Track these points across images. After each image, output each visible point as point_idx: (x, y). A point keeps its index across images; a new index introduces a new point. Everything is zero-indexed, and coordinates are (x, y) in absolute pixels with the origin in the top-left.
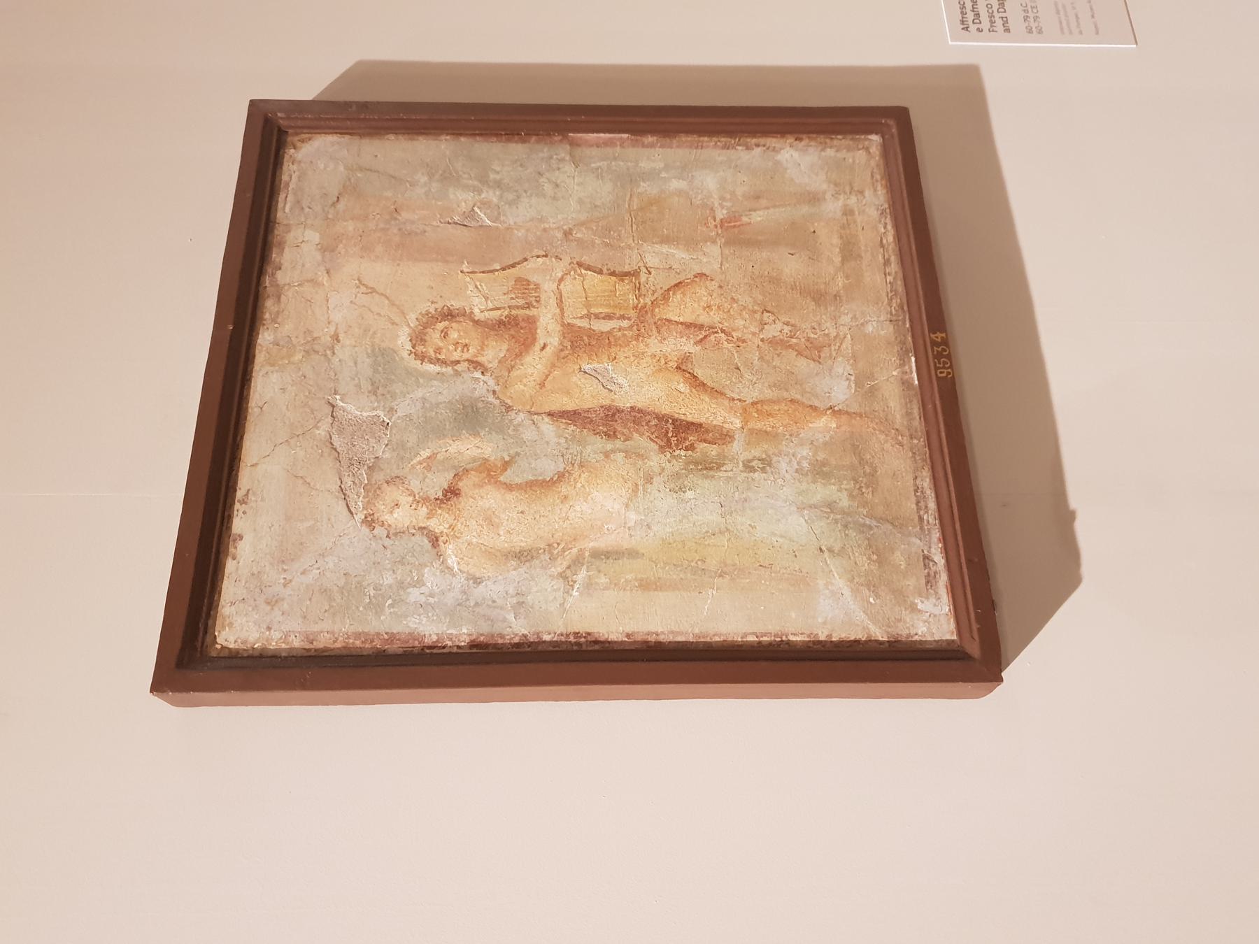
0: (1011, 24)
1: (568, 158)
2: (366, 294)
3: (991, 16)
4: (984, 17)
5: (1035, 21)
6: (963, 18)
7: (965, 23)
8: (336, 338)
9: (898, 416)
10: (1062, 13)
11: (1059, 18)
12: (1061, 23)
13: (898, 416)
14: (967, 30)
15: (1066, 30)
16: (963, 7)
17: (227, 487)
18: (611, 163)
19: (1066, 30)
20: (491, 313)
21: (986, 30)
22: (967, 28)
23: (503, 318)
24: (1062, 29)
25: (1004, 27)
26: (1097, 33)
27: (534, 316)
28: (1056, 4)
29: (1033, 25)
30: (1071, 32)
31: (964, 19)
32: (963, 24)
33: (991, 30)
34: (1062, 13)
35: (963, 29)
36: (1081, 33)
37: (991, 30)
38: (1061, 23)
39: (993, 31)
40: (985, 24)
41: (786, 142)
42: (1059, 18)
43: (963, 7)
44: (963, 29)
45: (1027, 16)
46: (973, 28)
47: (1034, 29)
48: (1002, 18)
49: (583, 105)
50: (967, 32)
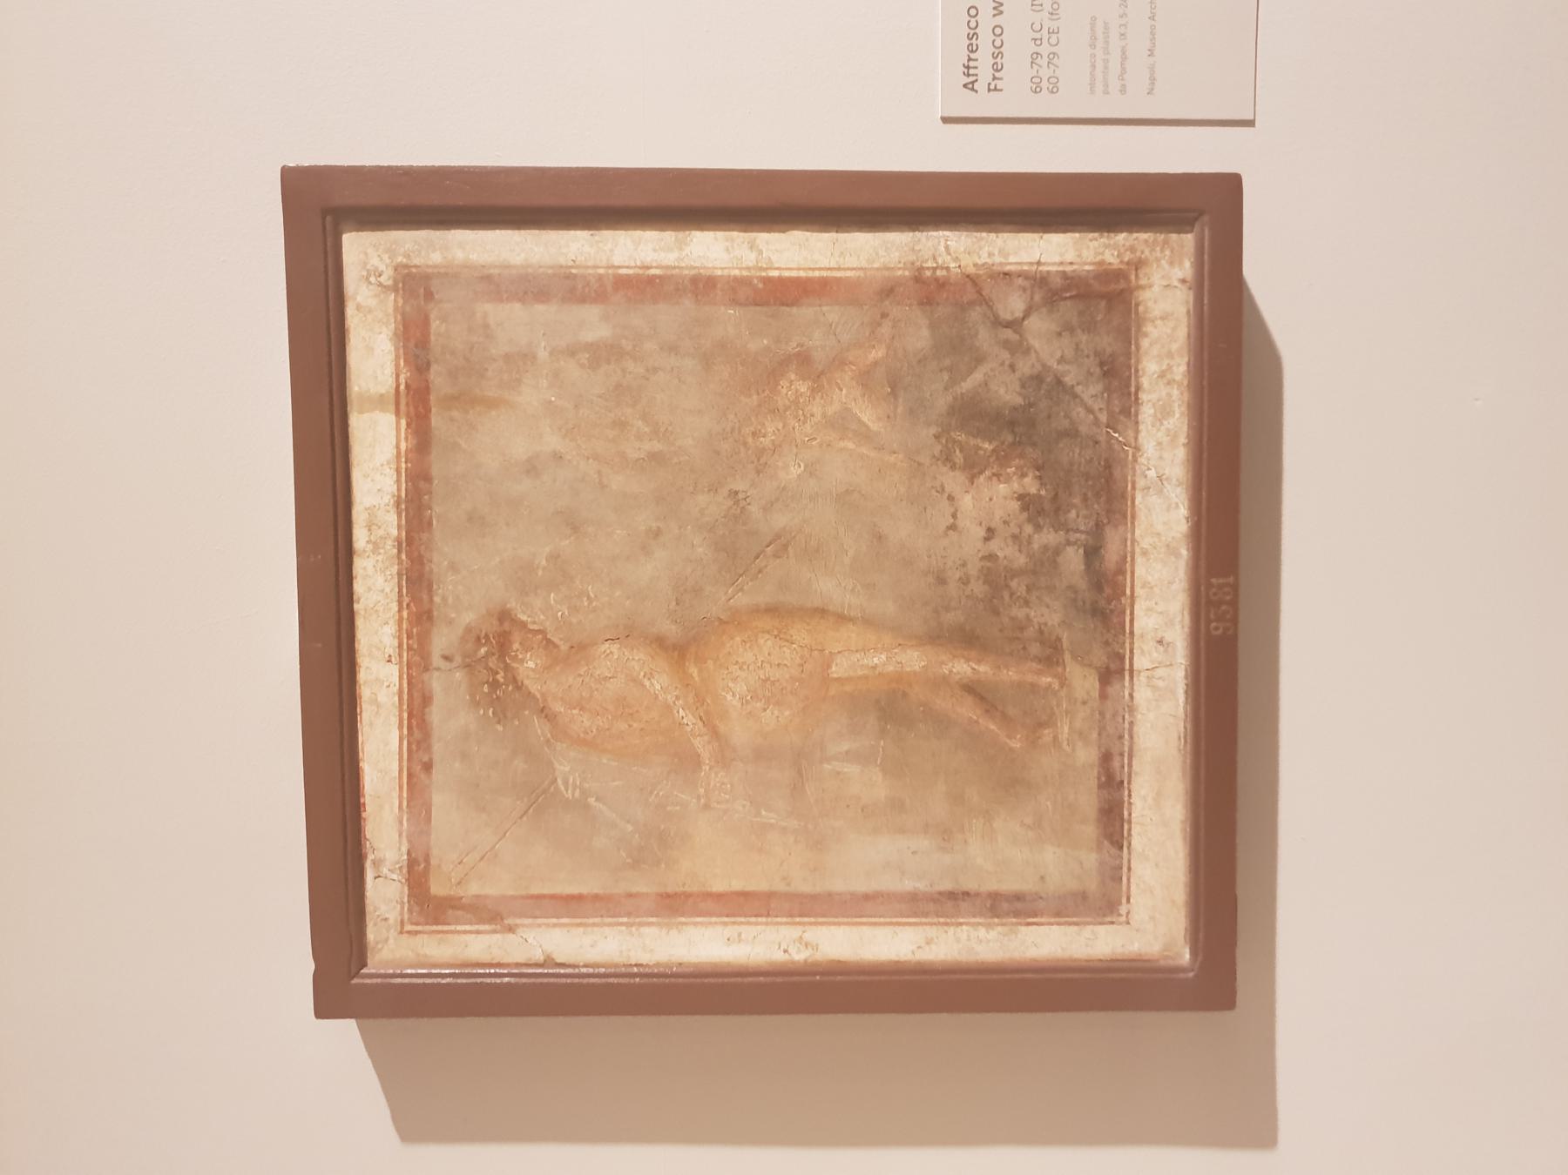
7: (971, 71)
8: (687, 578)
10: (1100, 44)
11: (1093, 56)
12: (1093, 66)
14: (973, 89)
15: (1099, 87)
16: (973, 12)
17: (841, 974)
19: (1099, 87)
22: (973, 83)
24: (1092, 85)
27: (973, 468)
28: (1094, 19)
29: (1045, 73)
30: (1106, 92)
31: (972, 64)
32: (968, 75)
33: (992, 87)
34: (1100, 44)
35: (965, 86)
36: (1123, 90)
37: (992, 87)
38: (1093, 66)
39: (995, 89)
42: (1093, 56)
43: (973, 12)
44: (965, 86)
47: (1044, 84)
48: (1036, 40)
49: (1137, 174)
50: (974, 93)
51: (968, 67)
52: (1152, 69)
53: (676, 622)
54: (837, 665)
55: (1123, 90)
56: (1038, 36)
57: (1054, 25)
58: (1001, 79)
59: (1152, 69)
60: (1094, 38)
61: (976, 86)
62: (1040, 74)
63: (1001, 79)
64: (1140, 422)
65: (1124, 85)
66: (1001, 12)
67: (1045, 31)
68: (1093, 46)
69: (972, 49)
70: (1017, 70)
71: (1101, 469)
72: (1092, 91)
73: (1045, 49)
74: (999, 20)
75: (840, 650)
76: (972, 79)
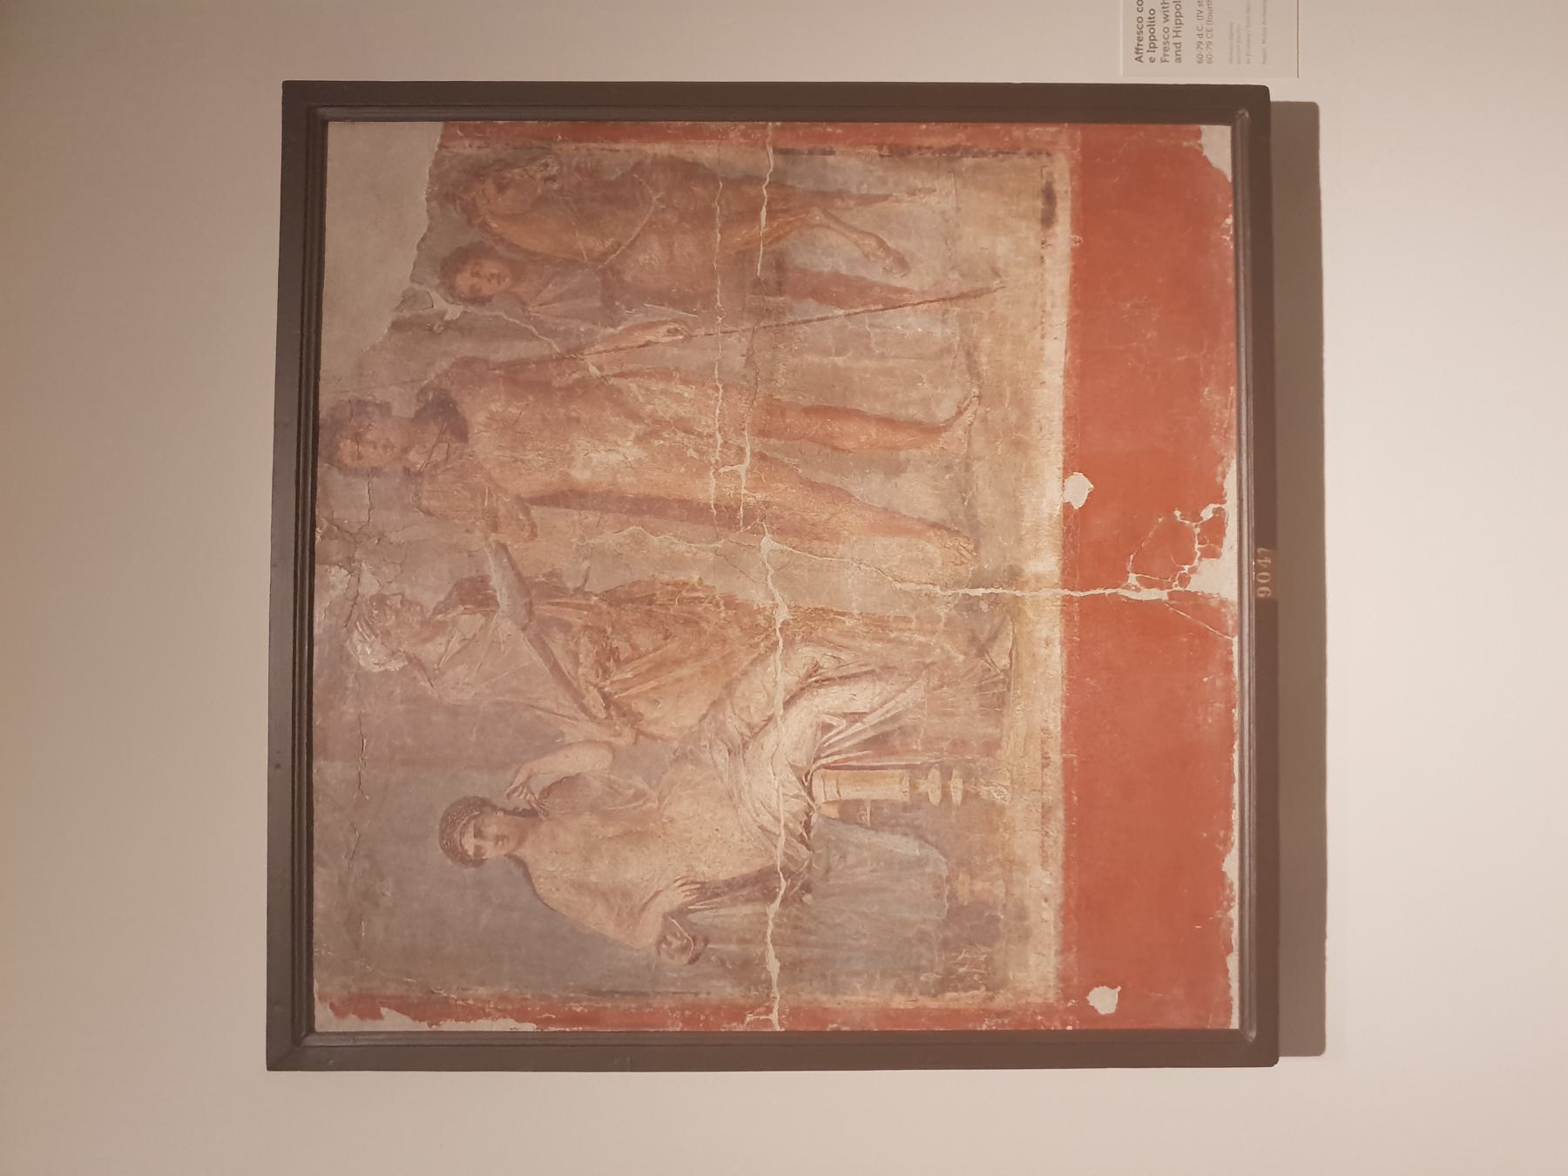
0: (1183, 54)
1: (327, 567)
2: (843, 614)
3: (1166, 42)
4: (1160, 44)
5: (1207, 47)
6: (1138, 45)
7: (1140, 51)
9: (351, 680)
13: (351, 680)
18: (582, 332)
20: (826, 315)
21: (1158, 61)
22: (1140, 57)
23: (568, 371)
25: (1177, 55)
26: (1264, 63)
30: (1239, 62)
31: (1140, 47)
32: (1137, 53)
35: (1136, 59)
36: (1248, 62)
38: (1231, 49)
39: (1165, 61)
40: (1159, 53)
41: (833, 267)
44: (1136, 59)
45: (1201, 42)
46: (1146, 58)
47: (1205, 58)
51: (1138, 49)
52: (1265, 29)
53: (967, 458)
54: (594, 706)
55: (1179, 60)
56: (1200, 33)
57: (1209, 27)
58: (1168, 55)
59: (1265, 29)
60: (1232, 34)
61: (1142, 59)
62: (1203, 53)
63: (1168, 55)
64: (1060, 548)
65: (1249, 59)
66: (1167, 20)
67: (1204, 30)
68: (1231, 38)
69: (1140, 40)
70: (1189, 52)
71: (1069, 645)
72: (1231, 61)
73: (1204, 40)
74: (1166, 24)
75: (451, 644)
76: (1139, 55)
